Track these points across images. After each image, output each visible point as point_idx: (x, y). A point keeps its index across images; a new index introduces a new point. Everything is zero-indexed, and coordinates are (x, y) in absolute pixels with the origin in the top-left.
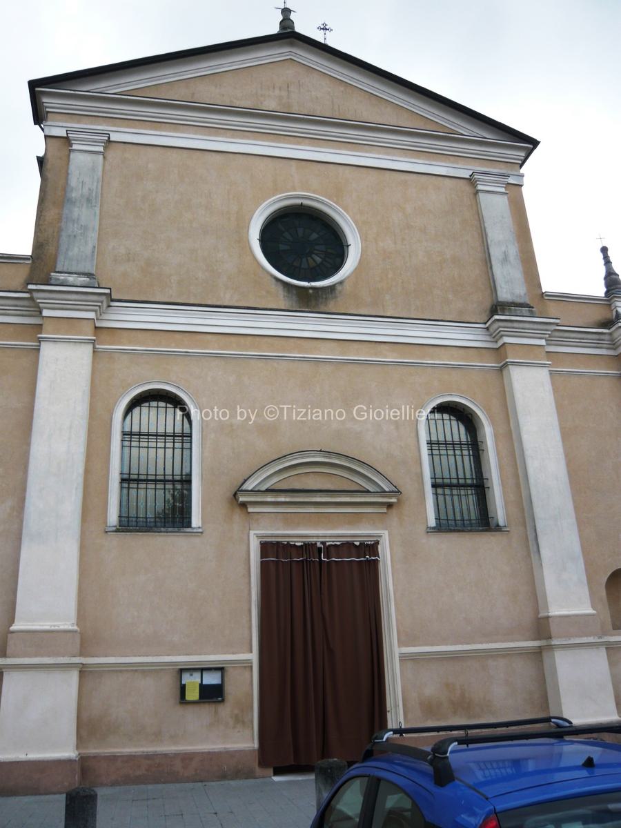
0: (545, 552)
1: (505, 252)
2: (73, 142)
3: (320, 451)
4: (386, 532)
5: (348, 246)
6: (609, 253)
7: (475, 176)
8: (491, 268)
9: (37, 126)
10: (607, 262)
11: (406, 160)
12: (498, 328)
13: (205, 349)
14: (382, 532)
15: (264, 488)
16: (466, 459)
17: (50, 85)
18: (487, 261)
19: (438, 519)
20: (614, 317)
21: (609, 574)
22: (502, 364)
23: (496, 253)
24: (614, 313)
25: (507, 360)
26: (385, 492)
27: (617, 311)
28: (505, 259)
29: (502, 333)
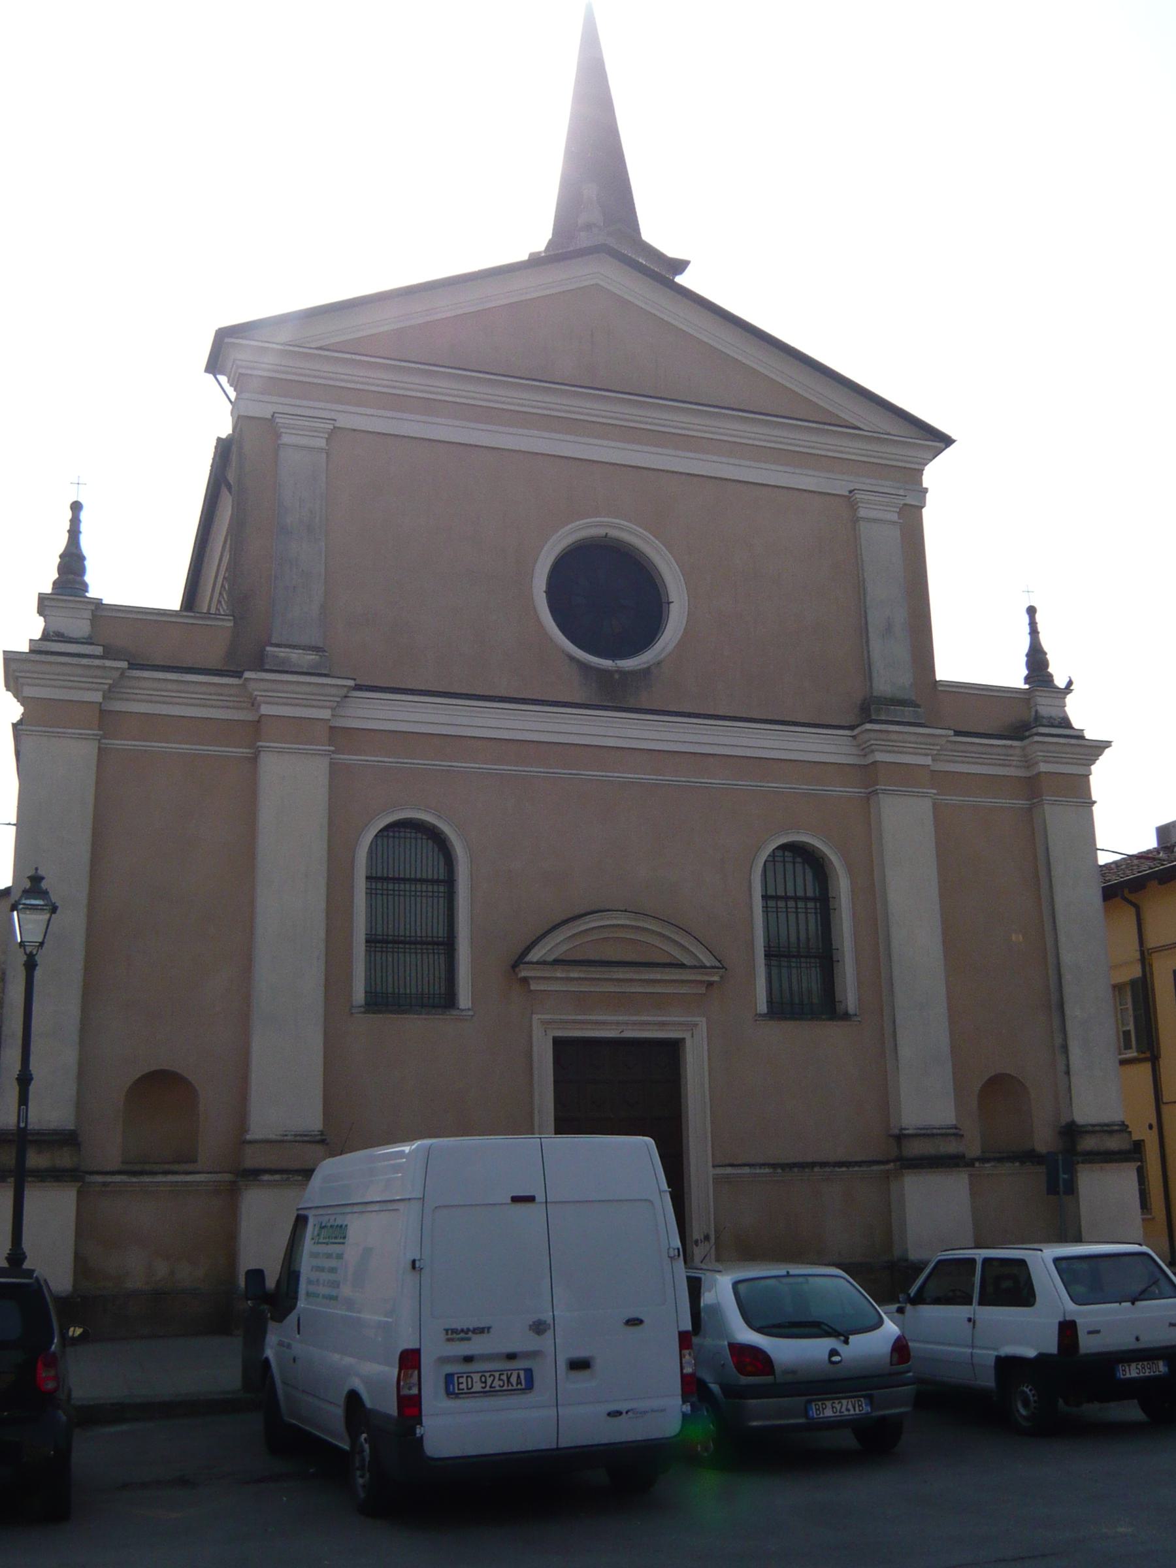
0: (905, 1052)
1: (889, 618)
2: (282, 430)
3: (626, 911)
4: (702, 1021)
5: (669, 603)
7: (857, 496)
8: (867, 642)
9: (211, 376)
10: (1034, 631)
12: (869, 741)
14: (698, 1019)
15: (551, 958)
16: (812, 918)
18: (863, 630)
19: (770, 1002)
20: (1032, 719)
21: (986, 1078)
22: (870, 790)
23: (876, 619)
24: (1033, 713)
25: (878, 787)
26: (705, 967)
27: (1036, 711)
28: (889, 629)
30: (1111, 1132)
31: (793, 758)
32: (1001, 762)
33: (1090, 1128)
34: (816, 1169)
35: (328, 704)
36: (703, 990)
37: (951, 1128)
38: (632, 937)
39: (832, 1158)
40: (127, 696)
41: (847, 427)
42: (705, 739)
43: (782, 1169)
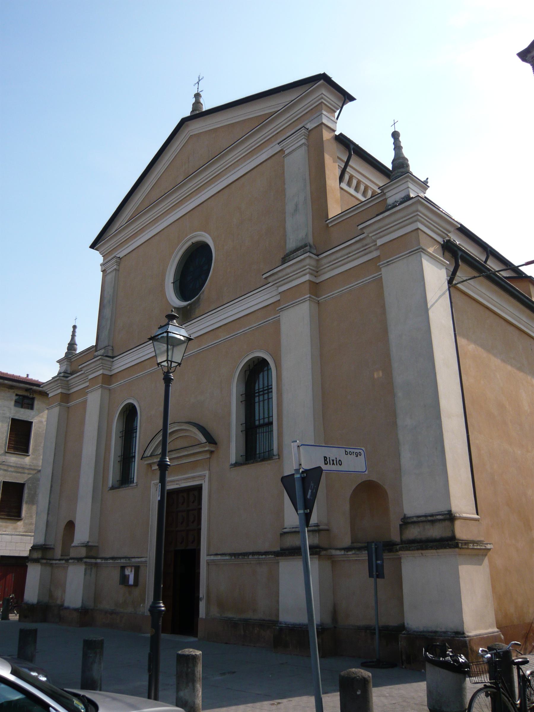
6: (77, 330)
10: (73, 335)
11: (210, 188)
13: (145, 371)
17: (98, 243)
28: (296, 210)
29: (419, 218)
30: (433, 522)
32: (362, 253)
33: (415, 519)
36: (208, 456)
38: (185, 434)
39: (263, 550)
40: (74, 386)
41: (276, 112)
42: (141, 355)
43: (235, 557)
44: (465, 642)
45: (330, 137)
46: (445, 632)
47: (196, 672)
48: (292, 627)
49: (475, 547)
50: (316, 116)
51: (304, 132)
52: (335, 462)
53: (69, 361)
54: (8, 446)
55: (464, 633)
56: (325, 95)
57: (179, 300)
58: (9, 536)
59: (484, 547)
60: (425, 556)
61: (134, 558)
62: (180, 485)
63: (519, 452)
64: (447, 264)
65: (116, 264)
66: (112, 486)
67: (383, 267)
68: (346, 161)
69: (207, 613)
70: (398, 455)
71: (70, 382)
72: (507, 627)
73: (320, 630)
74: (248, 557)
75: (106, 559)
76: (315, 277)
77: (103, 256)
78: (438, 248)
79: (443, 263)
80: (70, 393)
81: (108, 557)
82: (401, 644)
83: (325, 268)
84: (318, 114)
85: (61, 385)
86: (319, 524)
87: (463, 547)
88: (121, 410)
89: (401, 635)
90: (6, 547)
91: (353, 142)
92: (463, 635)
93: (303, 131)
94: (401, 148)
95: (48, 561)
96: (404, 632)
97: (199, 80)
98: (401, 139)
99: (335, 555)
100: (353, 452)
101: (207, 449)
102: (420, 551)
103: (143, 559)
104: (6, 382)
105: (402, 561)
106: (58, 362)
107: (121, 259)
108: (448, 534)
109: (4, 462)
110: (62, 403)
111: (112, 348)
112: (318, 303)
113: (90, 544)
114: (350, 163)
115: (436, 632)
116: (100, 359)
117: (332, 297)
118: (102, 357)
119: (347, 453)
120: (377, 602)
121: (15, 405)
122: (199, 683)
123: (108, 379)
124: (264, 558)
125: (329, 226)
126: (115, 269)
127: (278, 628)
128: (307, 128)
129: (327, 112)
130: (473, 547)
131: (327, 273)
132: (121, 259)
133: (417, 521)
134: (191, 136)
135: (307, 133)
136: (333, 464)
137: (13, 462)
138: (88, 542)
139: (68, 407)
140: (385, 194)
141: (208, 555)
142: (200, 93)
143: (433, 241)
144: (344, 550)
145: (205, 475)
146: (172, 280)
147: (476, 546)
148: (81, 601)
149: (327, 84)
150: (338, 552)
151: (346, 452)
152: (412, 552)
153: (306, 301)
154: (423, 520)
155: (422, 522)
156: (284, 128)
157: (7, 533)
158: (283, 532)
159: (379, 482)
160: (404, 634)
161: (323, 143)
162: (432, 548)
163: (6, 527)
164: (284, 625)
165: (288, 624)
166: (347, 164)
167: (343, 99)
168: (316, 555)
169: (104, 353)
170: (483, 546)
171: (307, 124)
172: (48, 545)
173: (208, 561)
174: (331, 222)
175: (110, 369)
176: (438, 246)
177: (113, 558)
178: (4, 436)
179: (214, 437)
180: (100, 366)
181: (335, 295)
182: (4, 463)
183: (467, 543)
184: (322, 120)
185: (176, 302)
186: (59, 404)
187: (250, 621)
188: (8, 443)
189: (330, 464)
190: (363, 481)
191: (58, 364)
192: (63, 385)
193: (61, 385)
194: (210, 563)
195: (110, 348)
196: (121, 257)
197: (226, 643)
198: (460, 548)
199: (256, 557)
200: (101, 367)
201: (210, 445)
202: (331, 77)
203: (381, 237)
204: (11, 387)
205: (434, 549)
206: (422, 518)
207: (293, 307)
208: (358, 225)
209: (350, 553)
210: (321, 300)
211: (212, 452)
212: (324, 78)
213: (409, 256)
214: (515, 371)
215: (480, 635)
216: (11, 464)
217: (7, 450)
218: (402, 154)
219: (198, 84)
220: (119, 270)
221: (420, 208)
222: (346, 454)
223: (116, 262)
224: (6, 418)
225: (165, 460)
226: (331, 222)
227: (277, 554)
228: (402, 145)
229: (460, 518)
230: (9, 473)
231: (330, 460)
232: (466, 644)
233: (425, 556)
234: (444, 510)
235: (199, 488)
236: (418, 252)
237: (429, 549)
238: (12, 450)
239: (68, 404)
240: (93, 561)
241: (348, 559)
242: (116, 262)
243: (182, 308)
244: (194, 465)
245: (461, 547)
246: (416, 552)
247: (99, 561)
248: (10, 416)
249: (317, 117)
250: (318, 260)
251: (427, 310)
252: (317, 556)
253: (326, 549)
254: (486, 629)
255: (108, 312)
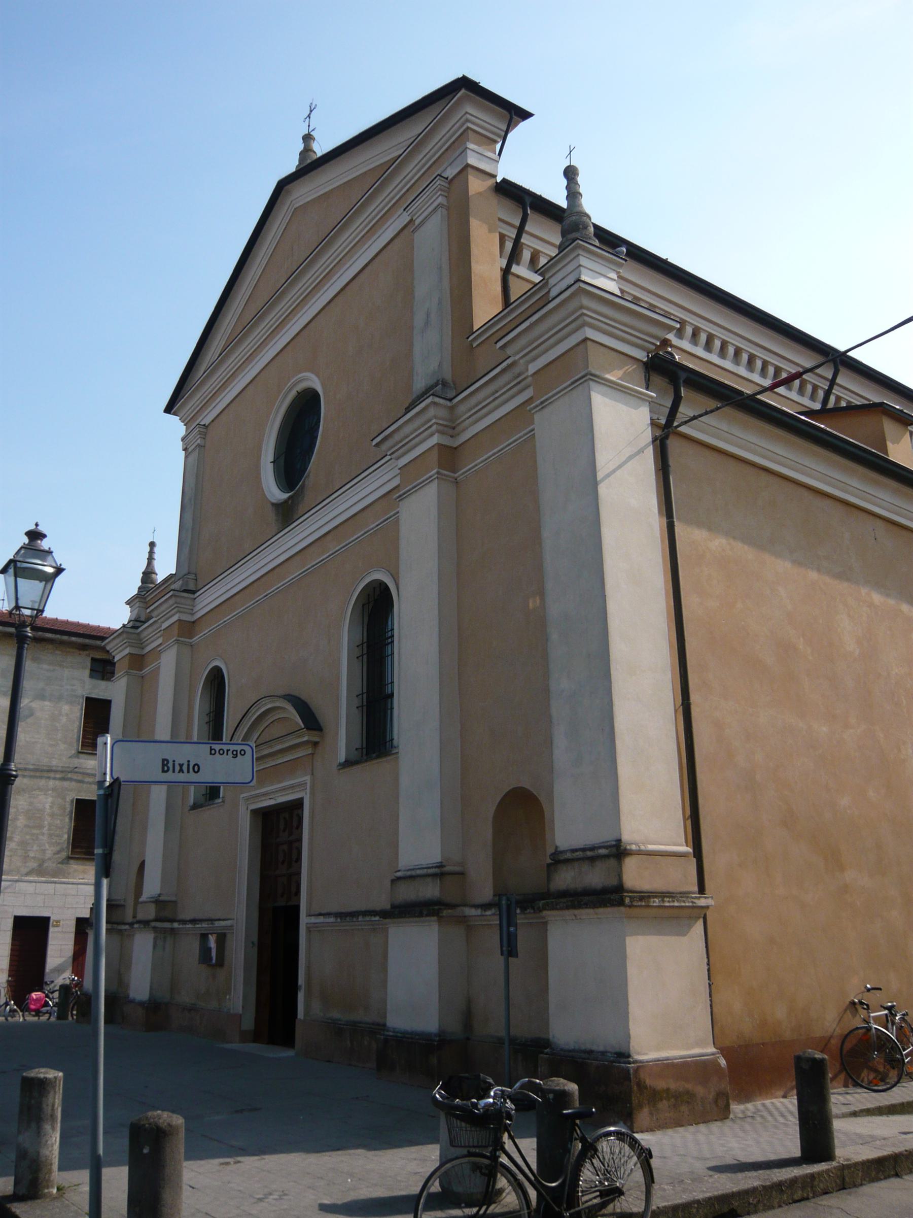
6: (156, 550)
10: (151, 559)
17: (178, 400)
28: (427, 323)
29: (586, 318)
30: (592, 859)
31: (388, 490)
33: (569, 855)
34: (360, 918)
35: (158, 635)
37: (432, 867)
41: (396, 160)
43: (341, 919)
44: (627, 1071)
45: (485, 188)
46: (603, 1053)
47: (44, 1106)
48: (401, 1037)
49: (667, 904)
50: (458, 153)
51: (440, 184)
52: (185, 768)
53: (142, 600)
54: (82, 742)
55: (629, 1056)
56: (472, 115)
57: (281, 491)
58: (89, 886)
59: (691, 904)
60: (580, 919)
61: (219, 920)
62: (276, 800)
63: (824, 729)
64: (652, 397)
65: (199, 436)
66: (194, 804)
67: (536, 411)
68: (518, 225)
69: (306, 1013)
70: (549, 742)
71: (143, 635)
72: (763, 1044)
73: (436, 1043)
74: (358, 919)
75: (184, 922)
76: (452, 436)
77: (185, 425)
78: (633, 370)
79: (643, 397)
80: (146, 652)
81: (188, 919)
82: (541, 1072)
83: (465, 420)
84: (461, 149)
85: (129, 641)
86: (444, 864)
87: (635, 904)
88: (206, 677)
89: (542, 1055)
90: (85, 903)
91: (531, 192)
92: (627, 1059)
93: (439, 182)
94: (578, 195)
95: (115, 926)
96: (547, 1050)
97: (311, 111)
98: (580, 179)
99: (470, 916)
100: (228, 750)
101: (306, 739)
102: (572, 911)
103: (228, 923)
104: (73, 639)
105: (549, 927)
106: (128, 603)
107: (207, 427)
108: (613, 882)
109: (76, 768)
110: (132, 671)
111: (196, 576)
112: (456, 482)
113: (162, 898)
114: (527, 228)
115: (591, 1052)
116: (171, 596)
117: (475, 470)
118: (176, 593)
119: (213, 752)
120: (509, 998)
121: (91, 676)
122: (50, 1123)
123: (187, 629)
124: (378, 920)
125: (474, 346)
126: (198, 445)
127: (382, 1037)
128: (446, 177)
129: (476, 144)
130: (662, 904)
131: (469, 429)
132: (207, 427)
133: (572, 857)
134: (295, 209)
135: (447, 185)
136: (181, 771)
137: (91, 767)
138: (159, 895)
139: (142, 677)
140: (547, 283)
141: (310, 916)
142: (311, 133)
143: (622, 357)
144: (482, 909)
145: (306, 783)
146: (271, 458)
147: (669, 902)
148: (148, 988)
149: (473, 95)
150: (473, 912)
151: (211, 749)
152: (560, 912)
153: (432, 480)
154: (580, 856)
155: (578, 859)
156: (417, 181)
157: (86, 881)
158: (395, 877)
159: (532, 790)
160: (546, 1054)
161: (469, 198)
162: (587, 905)
163: (84, 872)
164: (391, 1034)
165: (397, 1032)
166: (521, 230)
167: (508, 116)
168: (433, 916)
169: (182, 586)
170: (689, 902)
171: (446, 169)
172: (115, 900)
173: (308, 925)
174: (475, 339)
175: (191, 611)
176: (635, 366)
177: (194, 921)
178: (76, 726)
179: (320, 720)
180: (175, 608)
181: (479, 466)
182: (76, 770)
183: (645, 897)
184: (467, 160)
185: (277, 494)
186: (126, 672)
187: (360, 1025)
188: (82, 737)
189: (174, 771)
190: (511, 788)
191: (128, 606)
192: (131, 641)
193: (129, 641)
194: (311, 929)
195: (192, 577)
196: (207, 425)
197: (329, 1061)
198: (630, 907)
199: (368, 918)
200: (176, 609)
201: (310, 732)
202: (478, 82)
203: (534, 359)
204: (83, 647)
205: (590, 908)
206: (578, 853)
207: (415, 491)
208: (495, 341)
209: (489, 913)
210: (459, 477)
211: (316, 744)
212: (464, 84)
213: (572, 389)
214: (828, 580)
215: (667, 1059)
216: (89, 771)
217: (81, 749)
218: (580, 205)
219: (310, 118)
220: (204, 446)
221: (586, 301)
222: (211, 754)
223: (200, 433)
224: (77, 697)
225: (9, 767)
226: (475, 339)
227: (385, 914)
228: (581, 190)
229: (641, 853)
230: (85, 785)
231: (174, 765)
232: (629, 1074)
233: (580, 919)
234: (610, 839)
235: (298, 804)
236: (585, 381)
237: (583, 908)
238: (90, 748)
239: (141, 671)
240: (167, 925)
241: (488, 923)
242: (200, 434)
243: (282, 503)
244: (292, 767)
245: (630, 904)
246: (566, 912)
247: (176, 925)
248: (84, 694)
249: (459, 155)
250: (452, 408)
251: (595, 484)
252: (435, 918)
253: (452, 906)
254: (688, 1049)
255: (189, 516)
